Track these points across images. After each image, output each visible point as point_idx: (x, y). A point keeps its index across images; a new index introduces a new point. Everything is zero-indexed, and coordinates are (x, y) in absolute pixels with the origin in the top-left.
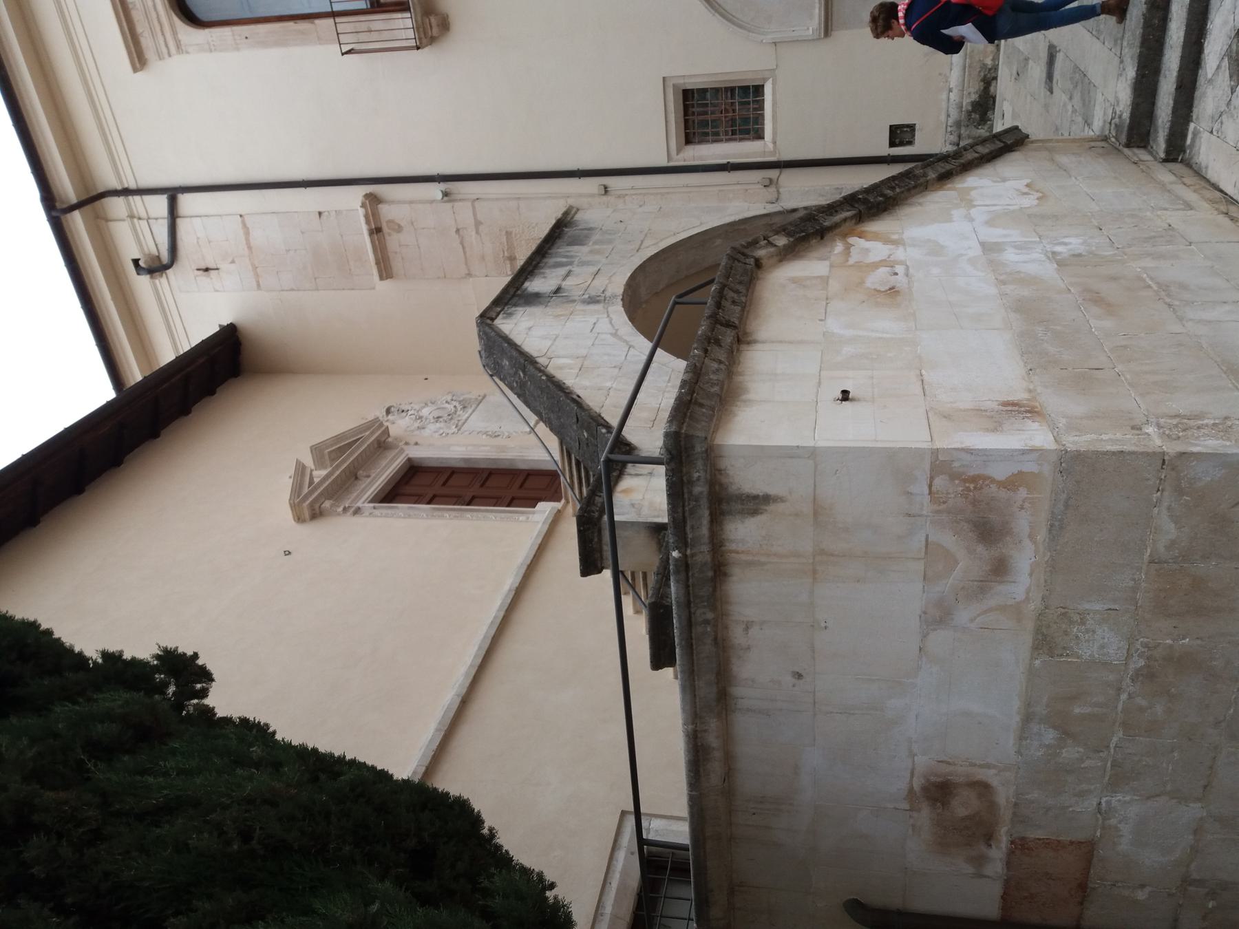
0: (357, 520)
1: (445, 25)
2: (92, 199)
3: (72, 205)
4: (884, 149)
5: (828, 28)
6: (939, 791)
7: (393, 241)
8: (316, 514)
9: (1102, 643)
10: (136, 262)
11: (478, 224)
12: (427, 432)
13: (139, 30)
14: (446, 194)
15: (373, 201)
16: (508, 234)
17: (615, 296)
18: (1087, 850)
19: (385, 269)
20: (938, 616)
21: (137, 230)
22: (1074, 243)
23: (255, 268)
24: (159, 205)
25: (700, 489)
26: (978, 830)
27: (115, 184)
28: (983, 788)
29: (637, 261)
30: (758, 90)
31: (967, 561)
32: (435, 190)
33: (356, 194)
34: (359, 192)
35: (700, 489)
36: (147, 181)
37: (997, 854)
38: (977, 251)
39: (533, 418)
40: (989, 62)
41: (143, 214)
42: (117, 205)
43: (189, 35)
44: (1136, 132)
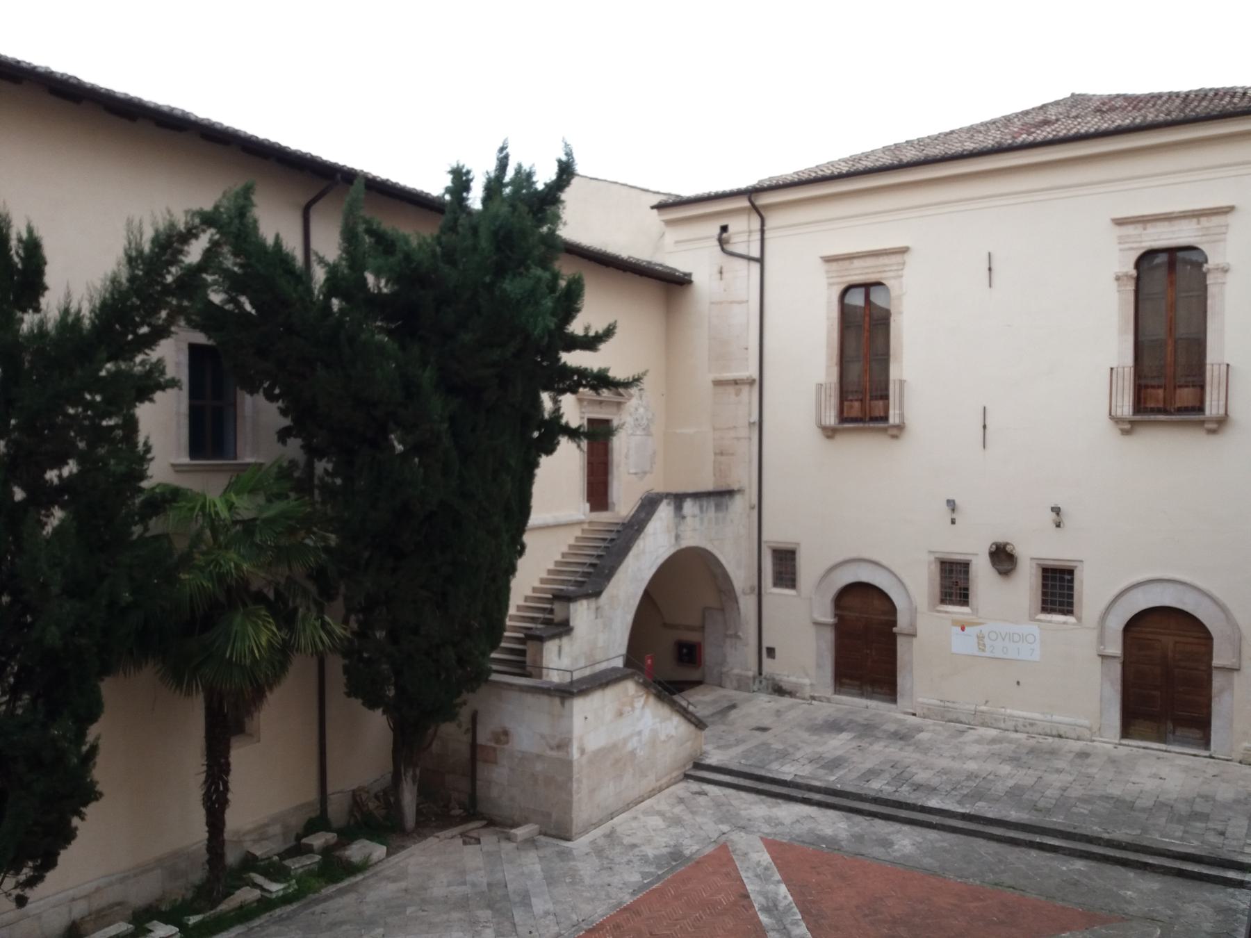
1: (829, 437)
3: (755, 199)
4: (765, 644)
5: (817, 624)
6: (506, 733)
7: (731, 390)
9: (539, 767)
11: (738, 439)
15: (751, 382)
18: (495, 762)
19: (718, 383)
20: (543, 737)
21: (743, 230)
22: (640, 753)
23: (721, 303)
26: (498, 741)
27: (769, 223)
28: (507, 742)
31: (554, 743)
32: (755, 418)
33: (756, 375)
37: (493, 744)
38: (637, 729)
39: (577, 675)
42: (756, 223)
44: (698, 766)
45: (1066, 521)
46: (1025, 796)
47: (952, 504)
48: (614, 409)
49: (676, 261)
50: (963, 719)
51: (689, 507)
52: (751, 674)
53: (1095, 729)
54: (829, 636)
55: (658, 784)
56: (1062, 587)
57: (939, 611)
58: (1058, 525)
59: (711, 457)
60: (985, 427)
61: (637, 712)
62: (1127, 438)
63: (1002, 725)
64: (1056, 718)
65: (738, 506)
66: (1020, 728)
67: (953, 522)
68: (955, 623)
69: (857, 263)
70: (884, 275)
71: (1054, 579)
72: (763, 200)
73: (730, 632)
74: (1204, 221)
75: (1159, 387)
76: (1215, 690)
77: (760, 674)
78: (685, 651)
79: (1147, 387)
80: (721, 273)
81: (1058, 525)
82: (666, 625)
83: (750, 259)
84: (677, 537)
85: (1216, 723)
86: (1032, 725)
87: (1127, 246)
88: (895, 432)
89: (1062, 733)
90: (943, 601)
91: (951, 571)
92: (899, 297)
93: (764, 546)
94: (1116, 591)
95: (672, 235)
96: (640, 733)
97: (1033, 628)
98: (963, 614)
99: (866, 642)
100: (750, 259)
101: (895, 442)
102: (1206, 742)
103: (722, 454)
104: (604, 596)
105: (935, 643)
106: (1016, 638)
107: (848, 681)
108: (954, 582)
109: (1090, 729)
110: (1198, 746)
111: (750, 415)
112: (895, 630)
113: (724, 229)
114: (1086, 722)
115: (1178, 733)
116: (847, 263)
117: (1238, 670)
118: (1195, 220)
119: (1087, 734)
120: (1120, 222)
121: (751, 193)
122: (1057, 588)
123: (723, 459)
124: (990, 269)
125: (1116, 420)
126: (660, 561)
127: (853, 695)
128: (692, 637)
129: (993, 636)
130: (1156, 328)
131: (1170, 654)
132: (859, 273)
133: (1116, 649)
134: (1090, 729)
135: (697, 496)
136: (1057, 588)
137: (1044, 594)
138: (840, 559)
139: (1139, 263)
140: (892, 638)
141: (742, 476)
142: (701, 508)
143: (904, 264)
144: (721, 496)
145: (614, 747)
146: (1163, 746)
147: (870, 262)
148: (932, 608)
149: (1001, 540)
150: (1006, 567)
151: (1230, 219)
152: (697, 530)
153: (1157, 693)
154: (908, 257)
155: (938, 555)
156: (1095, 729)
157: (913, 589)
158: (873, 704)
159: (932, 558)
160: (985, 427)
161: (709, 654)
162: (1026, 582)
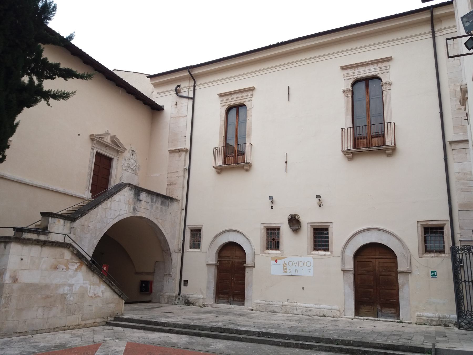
0: (90, 149)
2: (193, 78)
3: (192, 73)
4: (183, 279)
7: (177, 154)
8: (92, 140)
10: (179, 86)
11: (179, 177)
12: (123, 162)
13: (226, 97)
14: (186, 169)
15: (186, 151)
16: (176, 184)
17: (136, 214)
19: (171, 152)
23: (175, 117)
24: (191, 95)
25: (6, 240)
29: (152, 218)
30: (199, 248)
33: (188, 148)
34: (189, 148)
35: (6, 240)
36: (197, 92)
40: (197, 304)
41: (190, 90)
42: (192, 84)
43: (224, 109)
45: (324, 204)
46: (60, 307)
47: (271, 198)
48: (115, 154)
49: (159, 102)
50: (277, 310)
51: (143, 196)
52: (174, 295)
53: (342, 311)
54: (213, 271)
55: (84, 322)
56: (323, 237)
57: (266, 253)
58: (320, 206)
59: (166, 186)
60: (286, 163)
61: (71, 272)
62: (350, 162)
63: (296, 312)
64: (322, 306)
65: (175, 207)
66: (305, 313)
67: (272, 208)
68: (273, 259)
69: (233, 96)
70: (244, 100)
71: (319, 233)
72: (195, 72)
73: (167, 273)
74: (380, 65)
75: (364, 138)
76: (400, 285)
77: (179, 294)
78: (144, 285)
79: (358, 139)
80: (176, 105)
81: (320, 206)
82: (137, 273)
83: (189, 98)
84: (134, 209)
85: (402, 303)
86: (310, 310)
87: (348, 78)
88: (247, 167)
89: (325, 314)
90: (267, 249)
91: (271, 233)
92: (251, 109)
93: (187, 228)
94: (349, 236)
95: (156, 91)
96: (71, 285)
97: (310, 259)
98: (276, 254)
99: (231, 274)
100: (189, 98)
101: (247, 173)
102: (397, 315)
103: (170, 184)
104: (78, 222)
105: (266, 275)
106: (302, 264)
107: (222, 296)
108: (272, 238)
109: (339, 311)
110: (394, 318)
111: (185, 166)
112: (244, 265)
113: (179, 86)
114: (337, 308)
115: (383, 311)
116: (229, 97)
117: (410, 273)
118: (376, 65)
119: (338, 313)
120: (344, 68)
121: (189, 69)
122: (321, 238)
123: (170, 186)
124: (289, 94)
125: (345, 152)
126: (121, 218)
127: (224, 303)
128: (147, 278)
129: (290, 264)
130: (361, 122)
131: (377, 269)
132: (234, 100)
133: (350, 266)
134: (339, 311)
135: (149, 193)
136: (321, 238)
137: (315, 241)
138: (221, 231)
139: (353, 85)
140: (243, 269)
141: (179, 194)
142: (152, 200)
143: (253, 95)
144: (167, 199)
145: (47, 287)
146: (377, 319)
147: (238, 95)
148: (262, 252)
149: (293, 213)
150: (296, 227)
151: (390, 63)
152: (147, 210)
153: (372, 290)
154: (255, 93)
155: (265, 225)
156: (342, 311)
157: (253, 243)
158: (232, 306)
159: (263, 227)
160: (286, 163)
161: (156, 287)
162: (306, 234)
